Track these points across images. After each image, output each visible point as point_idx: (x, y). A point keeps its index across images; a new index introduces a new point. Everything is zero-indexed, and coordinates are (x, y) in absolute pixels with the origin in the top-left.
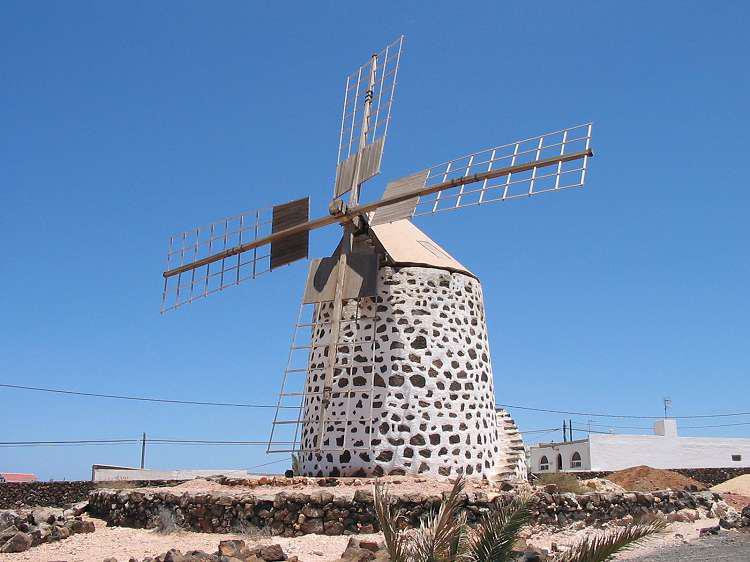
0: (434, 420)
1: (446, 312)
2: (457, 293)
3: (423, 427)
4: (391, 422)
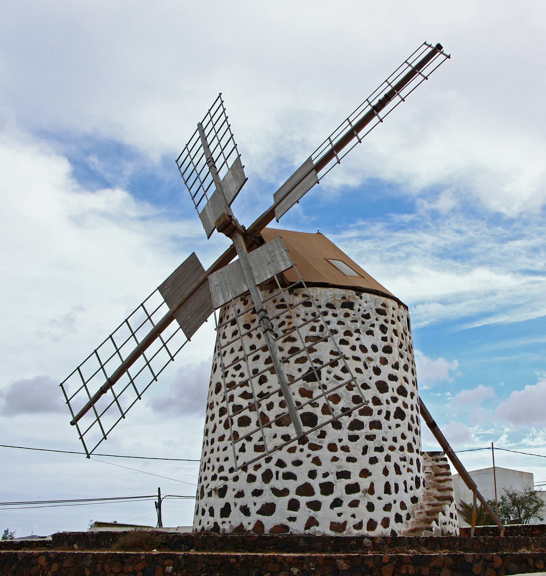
0: (327, 466)
1: (346, 338)
2: (363, 316)
3: (312, 474)
4: (274, 469)
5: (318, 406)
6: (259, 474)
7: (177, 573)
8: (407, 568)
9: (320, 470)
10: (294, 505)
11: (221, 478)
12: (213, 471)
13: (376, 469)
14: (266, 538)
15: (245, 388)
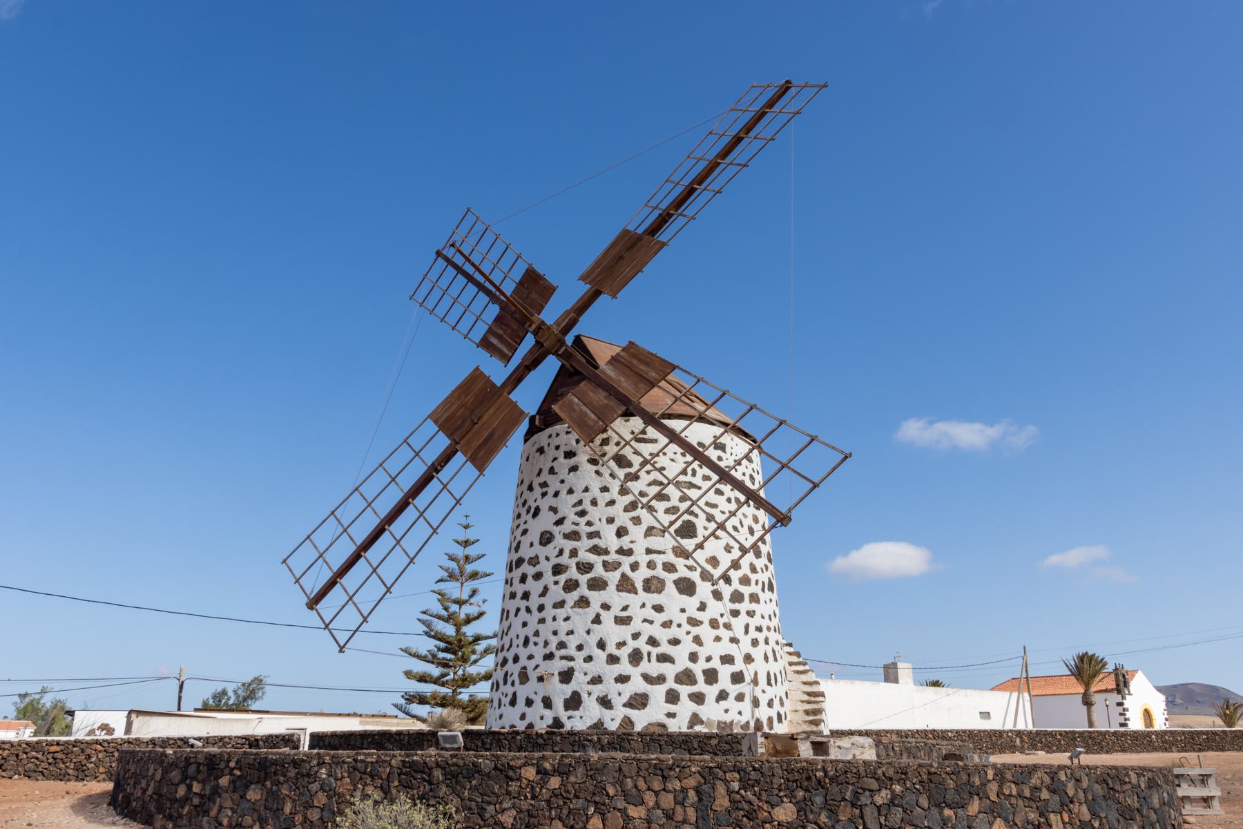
3: (693, 657)
4: (645, 648)
6: (623, 654)
9: (703, 652)
10: (672, 697)
11: (562, 658)
15: (595, 541)
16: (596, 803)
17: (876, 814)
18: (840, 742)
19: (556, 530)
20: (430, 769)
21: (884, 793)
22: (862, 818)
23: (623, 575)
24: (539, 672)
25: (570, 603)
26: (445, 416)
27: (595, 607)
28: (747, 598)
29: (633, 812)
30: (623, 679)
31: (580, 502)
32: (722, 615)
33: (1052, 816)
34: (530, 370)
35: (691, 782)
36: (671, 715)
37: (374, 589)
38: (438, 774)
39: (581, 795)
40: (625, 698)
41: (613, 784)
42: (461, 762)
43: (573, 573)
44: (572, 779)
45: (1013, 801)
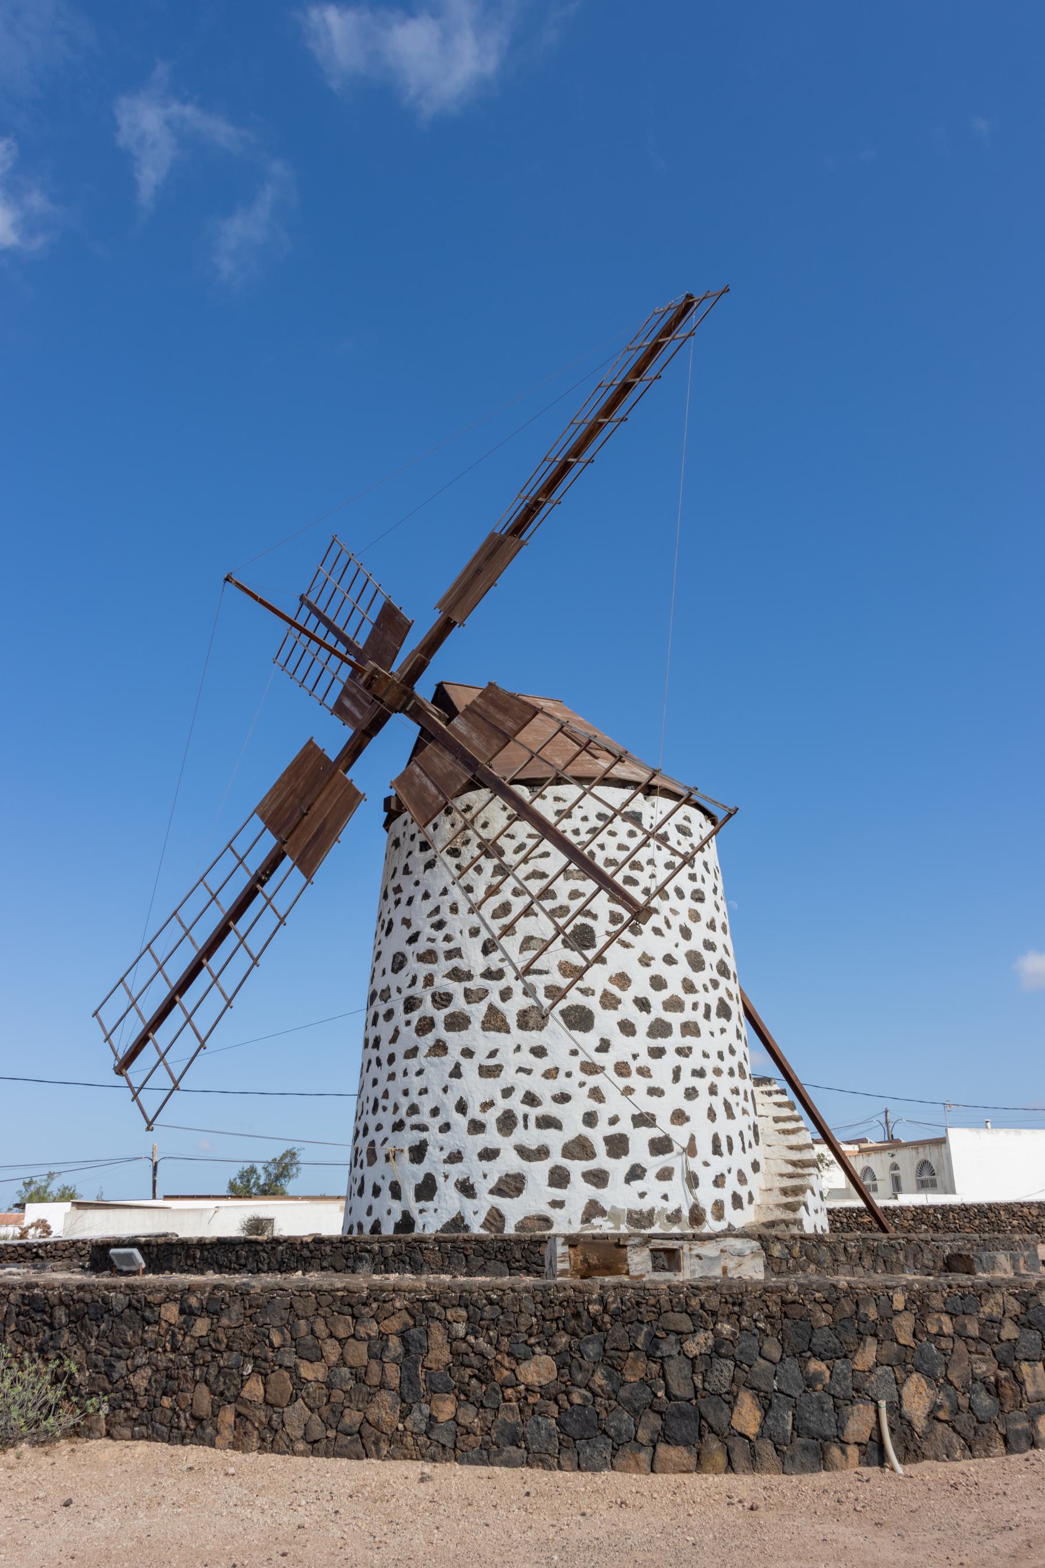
0: (615, 1104)
3: (590, 1119)
4: (521, 1109)
5: (593, 994)
6: (490, 1118)
7: (476, 1338)
8: (939, 1320)
9: (605, 1112)
10: (559, 1178)
11: (414, 1127)
12: (394, 1113)
13: (695, 1110)
14: (506, 1241)
15: (455, 962)
16: (255, 1358)
17: (687, 1371)
18: (699, 1249)
19: (409, 950)
20: (52, 1308)
21: (701, 1336)
22: (664, 1377)
23: (491, 1008)
24: (388, 1147)
25: (424, 1050)
26: (273, 809)
27: (455, 1053)
28: (676, 1029)
29: (307, 1371)
30: (489, 1154)
31: (437, 910)
32: (635, 1057)
33: (1025, 1367)
34: (371, 737)
35: (394, 1324)
36: (557, 1204)
37: (188, 1043)
38: (61, 1315)
39: (235, 1346)
40: (492, 1182)
41: (280, 1329)
42: (88, 1297)
43: (427, 1008)
44: (225, 1322)
45: (945, 1343)
